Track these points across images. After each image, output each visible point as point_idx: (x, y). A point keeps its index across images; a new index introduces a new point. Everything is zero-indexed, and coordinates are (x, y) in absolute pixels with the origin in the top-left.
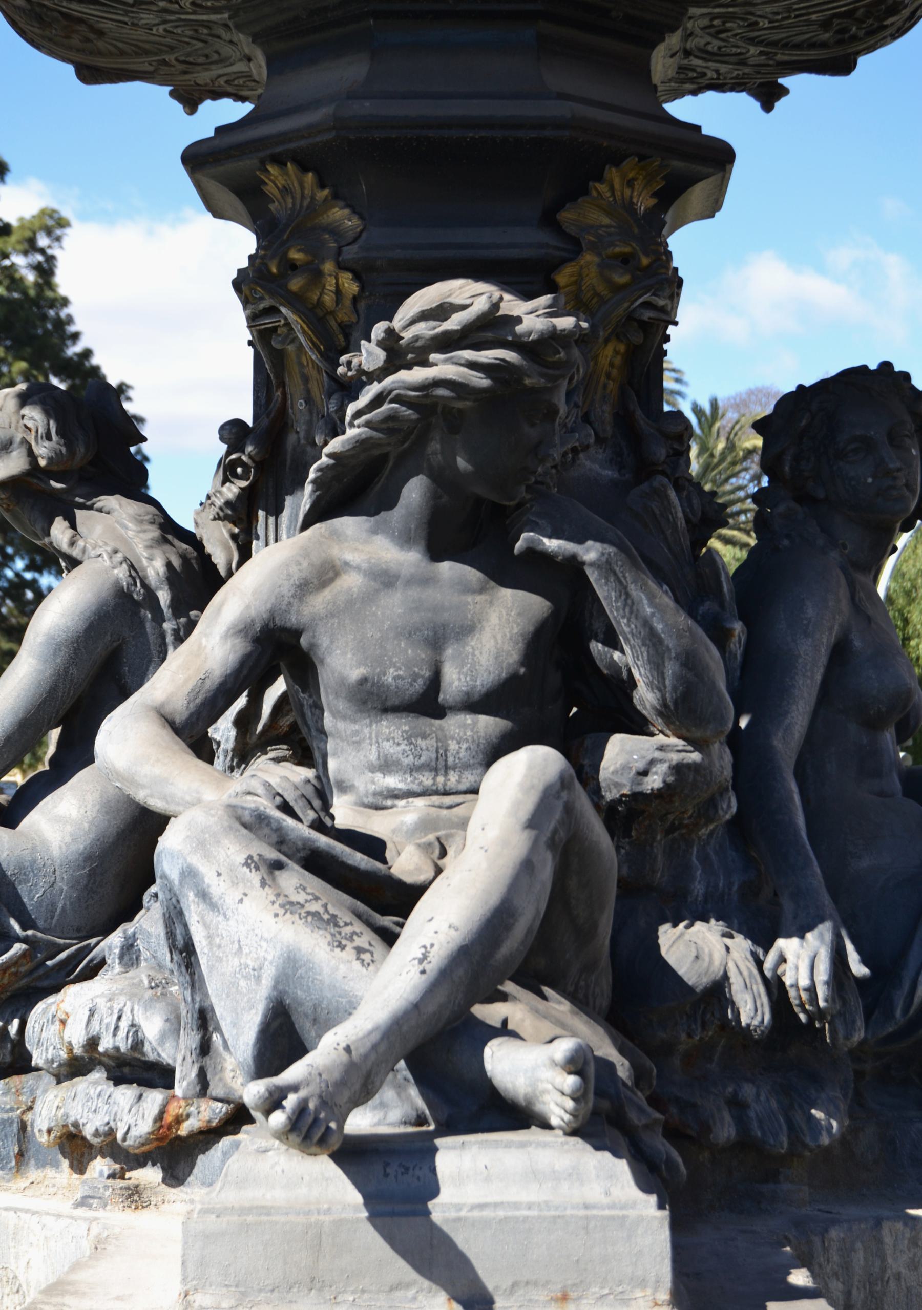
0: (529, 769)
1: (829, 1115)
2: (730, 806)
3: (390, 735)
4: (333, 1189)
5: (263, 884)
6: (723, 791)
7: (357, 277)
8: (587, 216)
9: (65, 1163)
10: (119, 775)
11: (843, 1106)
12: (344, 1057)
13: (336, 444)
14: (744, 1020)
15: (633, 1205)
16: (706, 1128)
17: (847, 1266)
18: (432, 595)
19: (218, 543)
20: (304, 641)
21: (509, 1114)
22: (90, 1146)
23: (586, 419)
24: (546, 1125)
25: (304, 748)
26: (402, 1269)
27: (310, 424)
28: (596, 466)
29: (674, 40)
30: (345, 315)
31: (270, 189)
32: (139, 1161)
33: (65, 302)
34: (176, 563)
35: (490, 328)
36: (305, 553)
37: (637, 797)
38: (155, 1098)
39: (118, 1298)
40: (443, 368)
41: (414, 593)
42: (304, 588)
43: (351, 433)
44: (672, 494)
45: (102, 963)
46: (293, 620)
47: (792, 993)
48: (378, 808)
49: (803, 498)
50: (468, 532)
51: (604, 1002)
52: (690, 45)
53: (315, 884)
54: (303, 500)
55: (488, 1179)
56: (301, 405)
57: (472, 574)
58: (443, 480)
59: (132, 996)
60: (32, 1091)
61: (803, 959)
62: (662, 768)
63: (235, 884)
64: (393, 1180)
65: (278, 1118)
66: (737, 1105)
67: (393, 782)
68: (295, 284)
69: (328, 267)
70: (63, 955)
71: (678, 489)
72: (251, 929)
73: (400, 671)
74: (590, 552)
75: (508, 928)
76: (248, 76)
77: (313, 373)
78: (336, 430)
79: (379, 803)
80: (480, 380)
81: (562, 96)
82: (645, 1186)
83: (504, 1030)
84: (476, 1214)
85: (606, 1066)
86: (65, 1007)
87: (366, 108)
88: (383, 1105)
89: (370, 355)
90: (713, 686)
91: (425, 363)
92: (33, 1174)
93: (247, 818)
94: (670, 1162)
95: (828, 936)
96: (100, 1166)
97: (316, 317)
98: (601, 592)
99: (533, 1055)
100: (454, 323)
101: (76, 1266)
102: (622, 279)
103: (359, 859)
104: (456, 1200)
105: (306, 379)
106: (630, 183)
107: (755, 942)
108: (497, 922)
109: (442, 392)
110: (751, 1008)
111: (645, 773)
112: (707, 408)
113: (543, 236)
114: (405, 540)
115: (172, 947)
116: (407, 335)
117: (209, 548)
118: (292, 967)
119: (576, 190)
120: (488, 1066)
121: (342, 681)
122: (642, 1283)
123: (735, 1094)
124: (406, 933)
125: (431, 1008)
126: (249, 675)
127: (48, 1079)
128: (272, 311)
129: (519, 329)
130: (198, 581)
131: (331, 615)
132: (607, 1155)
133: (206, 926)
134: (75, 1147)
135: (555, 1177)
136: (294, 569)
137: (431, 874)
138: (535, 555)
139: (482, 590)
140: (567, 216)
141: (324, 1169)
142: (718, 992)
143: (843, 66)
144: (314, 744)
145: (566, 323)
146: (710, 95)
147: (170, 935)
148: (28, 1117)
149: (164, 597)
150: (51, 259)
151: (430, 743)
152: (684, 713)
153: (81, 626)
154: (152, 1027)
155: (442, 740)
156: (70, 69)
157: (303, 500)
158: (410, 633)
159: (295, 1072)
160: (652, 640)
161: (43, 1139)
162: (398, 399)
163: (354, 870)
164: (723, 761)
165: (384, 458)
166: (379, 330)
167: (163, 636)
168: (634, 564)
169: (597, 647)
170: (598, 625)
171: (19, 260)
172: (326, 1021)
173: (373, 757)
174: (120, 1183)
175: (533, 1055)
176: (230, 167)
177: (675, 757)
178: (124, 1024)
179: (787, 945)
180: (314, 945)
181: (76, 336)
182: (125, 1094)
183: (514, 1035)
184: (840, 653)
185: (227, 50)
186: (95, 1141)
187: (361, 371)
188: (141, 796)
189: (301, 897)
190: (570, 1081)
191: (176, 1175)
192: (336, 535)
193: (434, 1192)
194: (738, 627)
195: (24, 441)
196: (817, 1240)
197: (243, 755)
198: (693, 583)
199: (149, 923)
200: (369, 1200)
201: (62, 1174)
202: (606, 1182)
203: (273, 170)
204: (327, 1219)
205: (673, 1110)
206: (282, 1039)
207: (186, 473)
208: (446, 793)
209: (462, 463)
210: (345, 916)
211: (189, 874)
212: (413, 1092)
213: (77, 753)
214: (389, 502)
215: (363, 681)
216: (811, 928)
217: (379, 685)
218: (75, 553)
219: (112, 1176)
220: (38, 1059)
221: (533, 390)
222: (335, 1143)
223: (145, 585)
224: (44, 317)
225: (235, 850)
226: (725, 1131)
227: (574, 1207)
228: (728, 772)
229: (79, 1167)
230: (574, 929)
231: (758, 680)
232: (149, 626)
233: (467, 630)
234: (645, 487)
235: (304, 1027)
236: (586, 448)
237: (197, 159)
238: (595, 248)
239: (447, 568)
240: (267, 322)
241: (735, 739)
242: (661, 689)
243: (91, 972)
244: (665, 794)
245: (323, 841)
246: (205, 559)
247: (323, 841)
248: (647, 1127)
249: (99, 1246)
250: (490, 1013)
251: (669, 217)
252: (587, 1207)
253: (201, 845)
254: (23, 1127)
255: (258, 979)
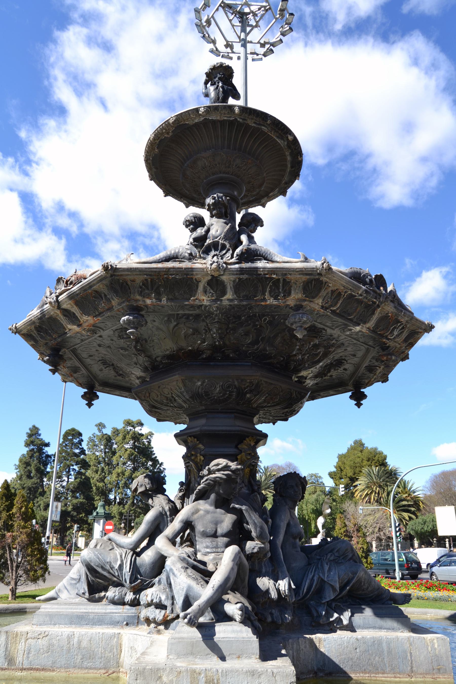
0: (232, 550)
1: (289, 616)
2: (269, 555)
3: (208, 541)
4: (195, 633)
5: (184, 572)
6: (268, 552)
7: (203, 457)
8: (243, 446)
9: (146, 624)
10: (159, 549)
11: (291, 614)
12: (198, 607)
13: (199, 487)
14: (272, 597)
15: (252, 638)
16: (266, 619)
17: (293, 648)
18: (216, 515)
19: (178, 505)
20: (193, 523)
21: (229, 618)
22: (151, 621)
23: (243, 482)
24: (236, 621)
25: (192, 545)
26: (208, 651)
27: (195, 483)
28: (245, 490)
29: (257, 416)
30: (201, 463)
31: (189, 441)
32: (160, 624)
33: (153, 448)
34: (171, 507)
35: (226, 468)
36: (193, 507)
37: (252, 553)
38: (163, 612)
39: (155, 656)
40: (218, 475)
41: (213, 515)
42: (193, 514)
43: (202, 485)
44: (258, 496)
45: (154, 584)
46: (191, 520)
47: (281, 591)
48: (205, 555)
49: (281, 496)
50: (222, 504)
51: (246, 594)
52: (260, 416)
53: (194, 572)
54: (193, 497)
55: (225, 632)
56: (193, 479)
57: (223, 511)
58: (218, 494)
59: (160, 591)
60: (141, 609)
61: (283, 585)
62: (257, 548)
63: (179, 572)
64: (207, 631)
65: (186, 620)
66: (271, 614)
67: (208, 550)
68: (193, 458)
69: (198, 455)
70: (147, 582)
71: (259, 494)
72: (182, 580)
73: (210, 529)
74: (244, 508)
75: (229, 581)
76: (185, 421)
77: (195, 473)
78: (199, 485)
79: (206, 554)
80: (224, 477)
81: (239, 426)
82: (254, 634)
83: (228, 601)
84: (222, 639)
85: (247, 608)
86: (147, 593)
87: (205, 428)
88: (205, 616)
89: (205, 472)
90: (266, 533)
91: (215, 474)
92: (140, 627)
93: (182, 559)
94: (259, 627)
95: (288, 580)
96: (153, 625)
97: (196, 464)
98: (246, 515)
99: (233, 608)
100: (220, 467)
101: (147, 648)
102: (249, 457)
103: (202, 567)
104: (219, 637)
105: (194, 475)
106: (250, 441)
107: (274, 581)
108: (227, 580)
109: (218, 479)
110: (274, 595)
111: (254, 549)
112: (266, 467)
113: (235, 450)
114: (211, 505)
115: (168, 583)
116: (212, 469)
117: (176, 504)
118: (189, 588)
119: (241, 442)
120: (225, 609)
121: (199, 531)
122: (254, 654)
123: (271, 612)
124: (210, 581)
125: (215, 597)
126: (183, 530)
127: (144, 607)
128: (189, 462)
129: (231, 468)
130: (175, 511)
131: (198, 519)
132: (247, 627)
133: (174, 580)
134: (148, 621)
135: (237, 632)
136: (191, 510)
137: (215, 569)
138: (234, 508)
139: (225, 514)
140: (239, 446)
141: (195, 630)
142: (268, 591)
143: (286, 420)
144: (194, 543)
145: (239, 467)
146: (264, 424)
147: (167, 581)
148: (139, 615)
149: (168, 513)
150: (150, 440)
151: (215, 543)
152: (261, 537)
153: (153, 519)
154: (163, 597)
155: (217, 542)
156: (155, 419)
157: (193, 497)
158: (212, 522)
159: (189, 611)
160: (255, 524)
161: (142, 620)
162: (210, 480)
163: (201, 569)
164: (268, 546)
165: (208, 490)
166: (207, 468)
167: (168, 521)
168: (252, 510)
169: (245, 525)
170: (245, 521)
171: (145, 440)
172: (196, 599)
173: (205, 545)
174: (156, 629)
175: (233, 608)
176: (182, 437)
177: (259, 546)
178: (158, 597)
179: (280, 582)
180: (193, 584)
181: (154, 454)
182: (158, 611)
183: (230, 602)
184: (288, 525)
185: (182, 417)
186: (152, 620)
187: (204, 475)
188: (163, 553)
189: (191, 574)
190: (240, 612)
191: (167, 628)
192: (199, 504)
193: (215, 635)
194: (270, 520)
195: (145, 485)
196: (287, 642)
197: (181, 544)
198: (262, 512)
199: (163, 576)
200: (203, 636)
201: (145, 627)
202: (247, 633)
203: (189, 438)
204: (195, 640)
205: (260, 615)
206: (187, 603)
207: (172, 489)
208: (218, 552)
209: (221, 491)
210: (199, 578)
211: (171, 570)
212: (211, 613)
213: (151, 543)
214: (208, 498)
215: (203, 531)
216: (284, 579)
217: (206, 532)
218: (153, 505)
219: (155, 628)
220: (142, 603)
221: (234, 478)
222: (196, 625)
223: (165, 511)
224: (149, 451)
225: (179, 565)
226: (269, 619)
227: (241, 638)
228: (269, 548)
229: (149, 625)
230: (242, 581)
231: (274, 530)
232: (165, 519)
233: (222, 522)
234: (253, 494)
235: (191, 600)
236: (243, 487)
237: (176, 436)
238: (244, 452)
239: (218, 510)
240: (188, 464)
241: (270, 542)
242: (256, 533)
243: (152, 586)
244: (257, 553)
245: (195, 563)
246: (176, 506)
247: (195, 563)
248: (255, 620)
249: (152, 643)
250: (225, 597)
251: (257, 446)
252: (243, 638)
253: (173, 564)
254: (138, 617)
255: (183, 590)
